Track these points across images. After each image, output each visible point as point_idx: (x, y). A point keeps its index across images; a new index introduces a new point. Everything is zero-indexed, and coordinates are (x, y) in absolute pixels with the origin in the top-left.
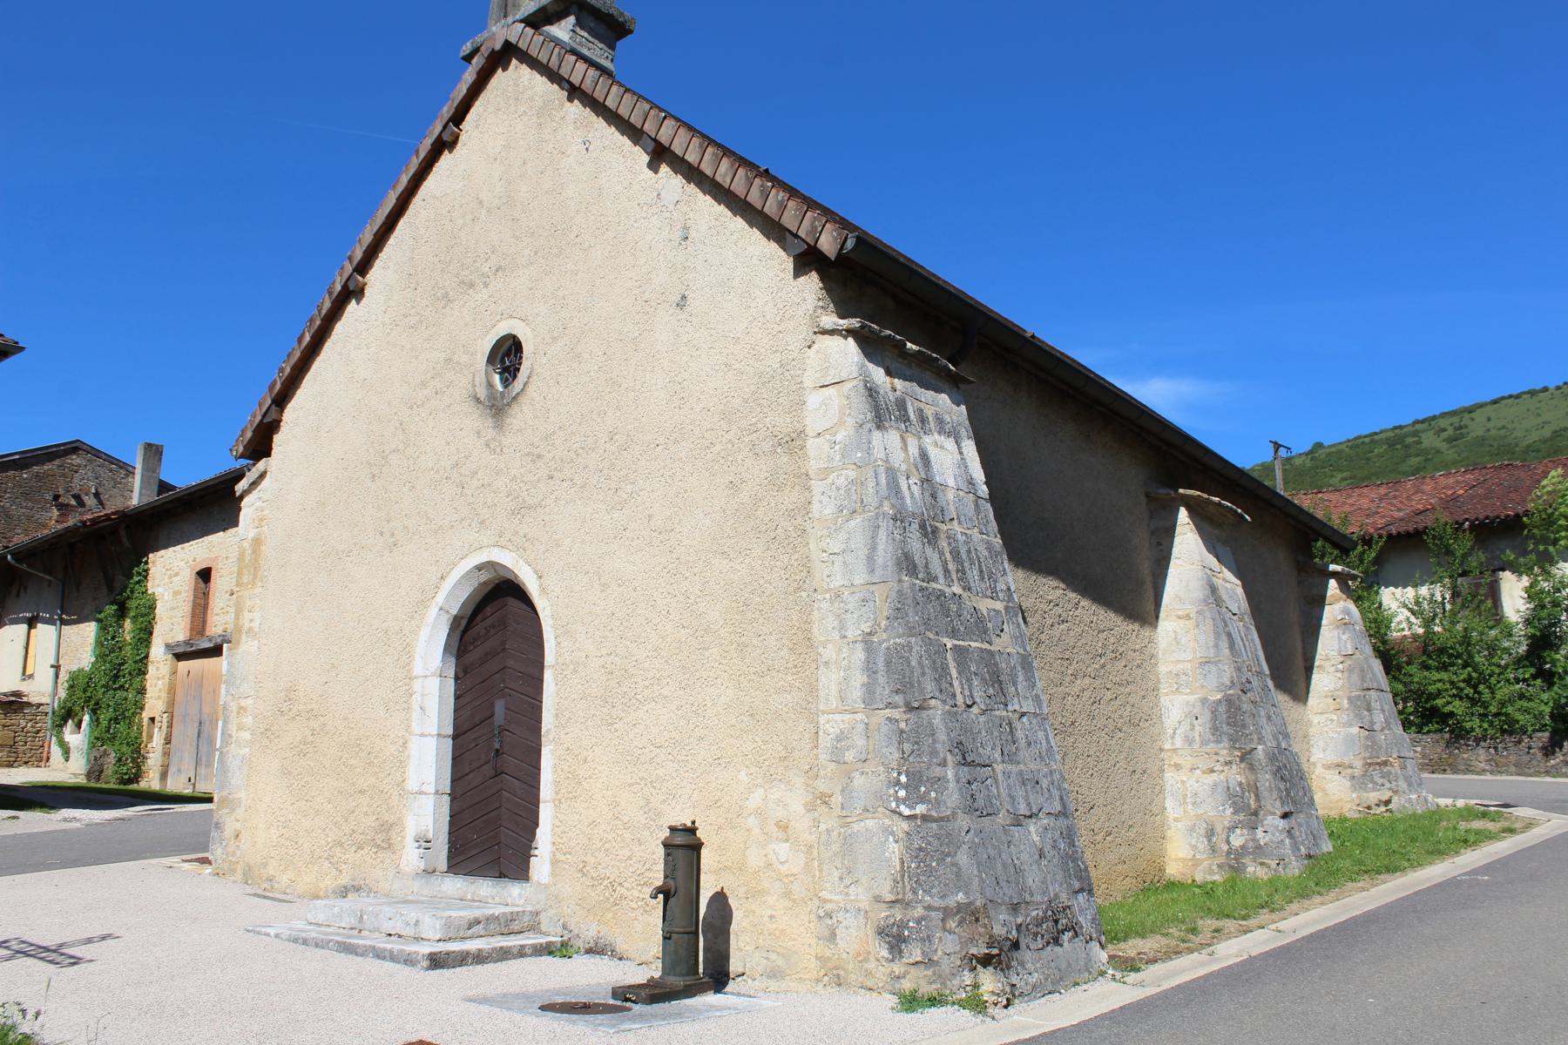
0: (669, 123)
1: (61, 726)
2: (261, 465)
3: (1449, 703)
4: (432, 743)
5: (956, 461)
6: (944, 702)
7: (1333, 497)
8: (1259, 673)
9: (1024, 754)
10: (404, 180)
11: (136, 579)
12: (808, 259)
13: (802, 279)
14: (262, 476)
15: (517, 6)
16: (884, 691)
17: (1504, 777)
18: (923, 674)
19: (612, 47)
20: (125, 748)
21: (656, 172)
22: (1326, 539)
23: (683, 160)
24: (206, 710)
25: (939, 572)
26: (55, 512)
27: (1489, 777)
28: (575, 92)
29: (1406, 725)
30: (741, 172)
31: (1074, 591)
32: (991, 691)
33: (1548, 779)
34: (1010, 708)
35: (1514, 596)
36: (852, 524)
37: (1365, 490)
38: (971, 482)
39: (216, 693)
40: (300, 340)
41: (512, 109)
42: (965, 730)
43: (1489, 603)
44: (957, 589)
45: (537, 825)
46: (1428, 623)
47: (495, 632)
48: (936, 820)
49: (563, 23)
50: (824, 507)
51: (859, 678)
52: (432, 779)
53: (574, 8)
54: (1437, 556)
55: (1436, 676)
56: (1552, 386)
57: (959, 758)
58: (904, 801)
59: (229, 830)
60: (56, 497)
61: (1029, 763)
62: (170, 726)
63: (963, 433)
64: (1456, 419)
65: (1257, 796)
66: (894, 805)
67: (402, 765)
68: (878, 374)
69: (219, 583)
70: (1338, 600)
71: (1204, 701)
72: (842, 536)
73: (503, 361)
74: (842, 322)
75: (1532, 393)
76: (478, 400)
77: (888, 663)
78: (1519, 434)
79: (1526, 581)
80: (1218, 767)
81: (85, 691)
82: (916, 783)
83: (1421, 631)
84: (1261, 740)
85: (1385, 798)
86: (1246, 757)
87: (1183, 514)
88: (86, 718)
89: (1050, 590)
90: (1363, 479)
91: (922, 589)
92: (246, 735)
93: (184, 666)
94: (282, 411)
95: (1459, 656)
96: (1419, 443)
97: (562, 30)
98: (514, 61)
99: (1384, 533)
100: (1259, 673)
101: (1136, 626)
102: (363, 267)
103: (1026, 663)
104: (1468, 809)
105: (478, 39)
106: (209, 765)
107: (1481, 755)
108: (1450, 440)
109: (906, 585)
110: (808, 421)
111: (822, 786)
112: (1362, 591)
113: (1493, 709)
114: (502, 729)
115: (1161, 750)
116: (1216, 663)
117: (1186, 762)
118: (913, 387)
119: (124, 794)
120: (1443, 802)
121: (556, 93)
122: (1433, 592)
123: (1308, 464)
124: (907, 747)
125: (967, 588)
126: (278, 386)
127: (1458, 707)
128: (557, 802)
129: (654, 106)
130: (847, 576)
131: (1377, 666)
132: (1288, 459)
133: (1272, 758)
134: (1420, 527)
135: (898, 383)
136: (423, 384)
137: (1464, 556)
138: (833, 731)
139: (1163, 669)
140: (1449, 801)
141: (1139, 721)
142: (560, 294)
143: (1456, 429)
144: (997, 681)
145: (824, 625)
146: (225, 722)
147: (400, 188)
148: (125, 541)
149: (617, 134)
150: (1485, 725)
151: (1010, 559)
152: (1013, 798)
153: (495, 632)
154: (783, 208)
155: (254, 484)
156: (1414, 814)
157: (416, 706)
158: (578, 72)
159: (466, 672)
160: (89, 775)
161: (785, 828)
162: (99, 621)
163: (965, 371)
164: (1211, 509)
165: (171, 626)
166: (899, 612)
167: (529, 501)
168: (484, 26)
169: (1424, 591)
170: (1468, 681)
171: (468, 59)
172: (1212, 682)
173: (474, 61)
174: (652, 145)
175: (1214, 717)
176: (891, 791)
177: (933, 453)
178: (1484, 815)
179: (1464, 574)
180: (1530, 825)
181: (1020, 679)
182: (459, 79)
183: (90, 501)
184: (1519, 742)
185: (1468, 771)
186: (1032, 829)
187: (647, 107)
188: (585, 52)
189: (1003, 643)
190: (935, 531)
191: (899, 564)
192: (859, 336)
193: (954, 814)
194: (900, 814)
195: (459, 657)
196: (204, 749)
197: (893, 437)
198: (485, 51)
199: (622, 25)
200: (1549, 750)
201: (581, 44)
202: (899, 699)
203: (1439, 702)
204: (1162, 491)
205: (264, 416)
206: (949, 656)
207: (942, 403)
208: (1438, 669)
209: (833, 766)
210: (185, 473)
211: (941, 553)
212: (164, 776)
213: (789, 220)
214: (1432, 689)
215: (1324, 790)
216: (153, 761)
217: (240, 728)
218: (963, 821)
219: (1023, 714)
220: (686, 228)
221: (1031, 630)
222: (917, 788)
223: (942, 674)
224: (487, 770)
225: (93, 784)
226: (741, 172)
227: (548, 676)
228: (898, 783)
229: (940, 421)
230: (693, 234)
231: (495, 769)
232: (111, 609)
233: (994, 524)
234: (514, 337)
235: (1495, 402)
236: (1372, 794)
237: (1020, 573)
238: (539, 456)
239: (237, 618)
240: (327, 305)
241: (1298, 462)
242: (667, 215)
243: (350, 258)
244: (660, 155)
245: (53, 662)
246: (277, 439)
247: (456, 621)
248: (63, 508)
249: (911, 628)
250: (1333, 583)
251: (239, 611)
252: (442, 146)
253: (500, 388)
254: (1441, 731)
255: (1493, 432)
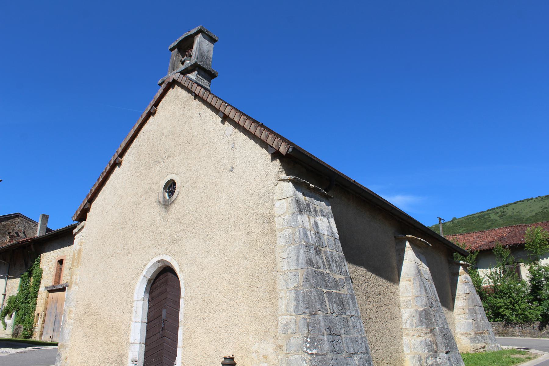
0: (229, 108)
1: (4, 317)
2: (83, 223)
3: (504, 311)
4: (139, 325)
5: (327, 226)
6: (323, 312)
7: (460, 237)
8: (436, 300)
9: (352, 331)
10: (137, 125)
11: (36, 263)
12: (276, 155)
13: (274, 162)
14: (83, 227)
15: (178, 67)
16: (302, 308)
17: (526, 338)
18: (316, 302)
19: (210, 81)
20: (27, 325)
21: (224, 124)
22: (458, 252)
23: (233, 120)
24: (58, 311)
25: (321, 265)
26: (9, 238)
27: (520, 338)
28: (196, 97)
29: (489, 319)
30: (253, 124)
31: (370, 271)
32: (340, 308)
33: (542, 339)
34: (347, 314)
35: (525, 272)
36: (291, 248)
37: (471, 234)
38: (333, 233)
39: (62, 305)
40: (98, 180)
41: (175, 102)
42: (331, 322)
43: (517, 274)
44: (328, 271)
45: (176, 356)
46: (495, 281)
47: (163, 285)
48: (320, 355)
49: (193, 73)
50: (281, 242)
51: (293, 303)
52: (139, 338)
53: (197, 68)
54: (497, 258)
55: (499, 300)
56: (534, 197)
57: (329, 332)
58: (309, 348)
59: (63, 357)
60: (9, 233)
61: (354, 334)
62: (45, 317)
63: (330, 216)
64: (502, 209)
65: (436, 345)
66: (305, 349)
67: (128, 333)
68: (300, 195)
69: (66, 265)
70: (463, 274)
71: (416, 311)
72: (287, 252)
73: (169, 189)
74: (287, 177)
75: (528, 200)
76: (160, 202)
77: (303, 298)
78: (524, 214)
79: (528, 267)
80: (422, 335)
81: (14, 304)
82: (313, 341)
83: (493, 284)
84: (437, 325)
85: (483, 346)
86: (432, 331)
87: (408, 244)
88: (14, 314)
89: (361, 271)
90: (470, 230)
91: (315, 271)
92: (72, 321)
93: (50, 294)
94: (91, 205)
95: (507, 294)
96: (489, 217)
97: (193, 76)
98: (176, 86)
99: (478, 250)
100: (436, 300)
101: (392, 284)
102: (121, 155)
103: (353, 298)
104: (513, 350)
105: (164, 78)
106: (58, 331)
107: (517, 330)
108: (500, 216)
109: (309, 270)
110: (275, 211)
111: (279, 342)
112: (472, 271)
113: (520, 312)
114: (165, 320)
115: (402, 329)
116: (420, 297)
117: (411, 333)
118: (312, 200)
119: (26, 342)
120: (504, 347)
121: (190, 97)
122: (497, 270)
123: (451, 225)
124: (310, 328)
125: (331, 271)
126: (90, 196)
127: (507, 312)
128: (184, 347)
129: (224, 101)
130: (288, 268)
131: (478, 297)
132: (444, 223)
133: (442, 332)
134: (491, 247)
135: (307, 198)
136: (141, 196)
137: (507, 258)
138: (284, 322)
139: (401, 299)
140: (506, 347)
141: (394, 317)
142: (190, 165)
143: (502, 212)
144: (342, 304)
145: (280, 284)
146: (64, 316)
147: (135, 128)
148: (33, 249)
149: (211, 111)
150: (518, 319)
151: (347, 260)
152: (348, 347)
153: (163, 285)
154: (267, 137)
155: (80, 230)
156: (494, 352)
157: (134, 312)
158: (198, 90)
159: (152, 299)
160: (13, 335)
161: (266, 358)
162: (21, 278)
163: (330, 194)
164: (418, 242)
165: (47, 280)
166: (307, 280)
167: (177, 238)
168: (166, 74)
169: (493, 270)
170: (510, 303)
171: (160, 85)
172: (419, 304)
173: (163, 85)
174: (222, 115)
175: (420, 317)
176: (304, 344)
177: (319, 223)
178: (519, 352)
179: (508, 264)
180: (536, 356)
181: (351, 303)
182: (157, 92)
183: (21, 234)
184: (530, 325)
185: (512, 335)
186: (355, 358)
187: (221, 102)
188: (200, 83)
189: (344, 291)
190: (320, 250)
191: (307, 262)
192: (294, 182)
193: (327, 353)
194: (308, 353)
195: (150, 294)
196: (56, 325)
197: (305, 217)
198: (166, 82)
199: (214, 74)
200: (541, 329)
201: (199, 80)
202: (307, 311)
203: (501, 310)
204: (400, 236)
205: (84, 206)
206: (325, 295)
207: (322, 205)
208: (499, 298)
209: (283, 335)
210: (56, 225)
211: (322, 258)
212: (41, 335)
213: (269, 141)
214: (498, 305)
215: (461, 343)
216: (38, 330)
217: (70, 318)
218: (330, 356)
219: (352, 316)
220: (233, 144)
221: (354, 285)
222: (314, 343)
223: (322, 302)
224: (159, 335)
225: (14, 339)
226: (253, 124)
227: (182, 301)
228: (307, 341)
229: (322, 211)
230: (236, 146)
231: (162, 335)
232: (26, 274)
233: (341, 248)
234: (173, 180)
235: (515, 203)
236: (478, 344)
237: (350, 265)
238: (181, 222)
239: (71, 278)
240: (108, 168)
241: (448, 224)
242: (227, 139)
243: (117, 152)
244: (225, 118)
245: (3, 293)
246: (89, 214)
247: (149, 280)
248: (12, 237)
249: (311, 285)
250: (461, 268)
251: (72, 276)
252: (151, 114)
253: (168, 198)
254: (502, 321)
255: (515, 214)
